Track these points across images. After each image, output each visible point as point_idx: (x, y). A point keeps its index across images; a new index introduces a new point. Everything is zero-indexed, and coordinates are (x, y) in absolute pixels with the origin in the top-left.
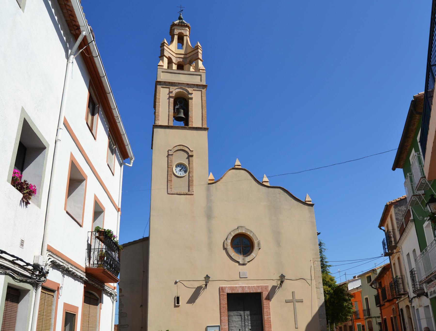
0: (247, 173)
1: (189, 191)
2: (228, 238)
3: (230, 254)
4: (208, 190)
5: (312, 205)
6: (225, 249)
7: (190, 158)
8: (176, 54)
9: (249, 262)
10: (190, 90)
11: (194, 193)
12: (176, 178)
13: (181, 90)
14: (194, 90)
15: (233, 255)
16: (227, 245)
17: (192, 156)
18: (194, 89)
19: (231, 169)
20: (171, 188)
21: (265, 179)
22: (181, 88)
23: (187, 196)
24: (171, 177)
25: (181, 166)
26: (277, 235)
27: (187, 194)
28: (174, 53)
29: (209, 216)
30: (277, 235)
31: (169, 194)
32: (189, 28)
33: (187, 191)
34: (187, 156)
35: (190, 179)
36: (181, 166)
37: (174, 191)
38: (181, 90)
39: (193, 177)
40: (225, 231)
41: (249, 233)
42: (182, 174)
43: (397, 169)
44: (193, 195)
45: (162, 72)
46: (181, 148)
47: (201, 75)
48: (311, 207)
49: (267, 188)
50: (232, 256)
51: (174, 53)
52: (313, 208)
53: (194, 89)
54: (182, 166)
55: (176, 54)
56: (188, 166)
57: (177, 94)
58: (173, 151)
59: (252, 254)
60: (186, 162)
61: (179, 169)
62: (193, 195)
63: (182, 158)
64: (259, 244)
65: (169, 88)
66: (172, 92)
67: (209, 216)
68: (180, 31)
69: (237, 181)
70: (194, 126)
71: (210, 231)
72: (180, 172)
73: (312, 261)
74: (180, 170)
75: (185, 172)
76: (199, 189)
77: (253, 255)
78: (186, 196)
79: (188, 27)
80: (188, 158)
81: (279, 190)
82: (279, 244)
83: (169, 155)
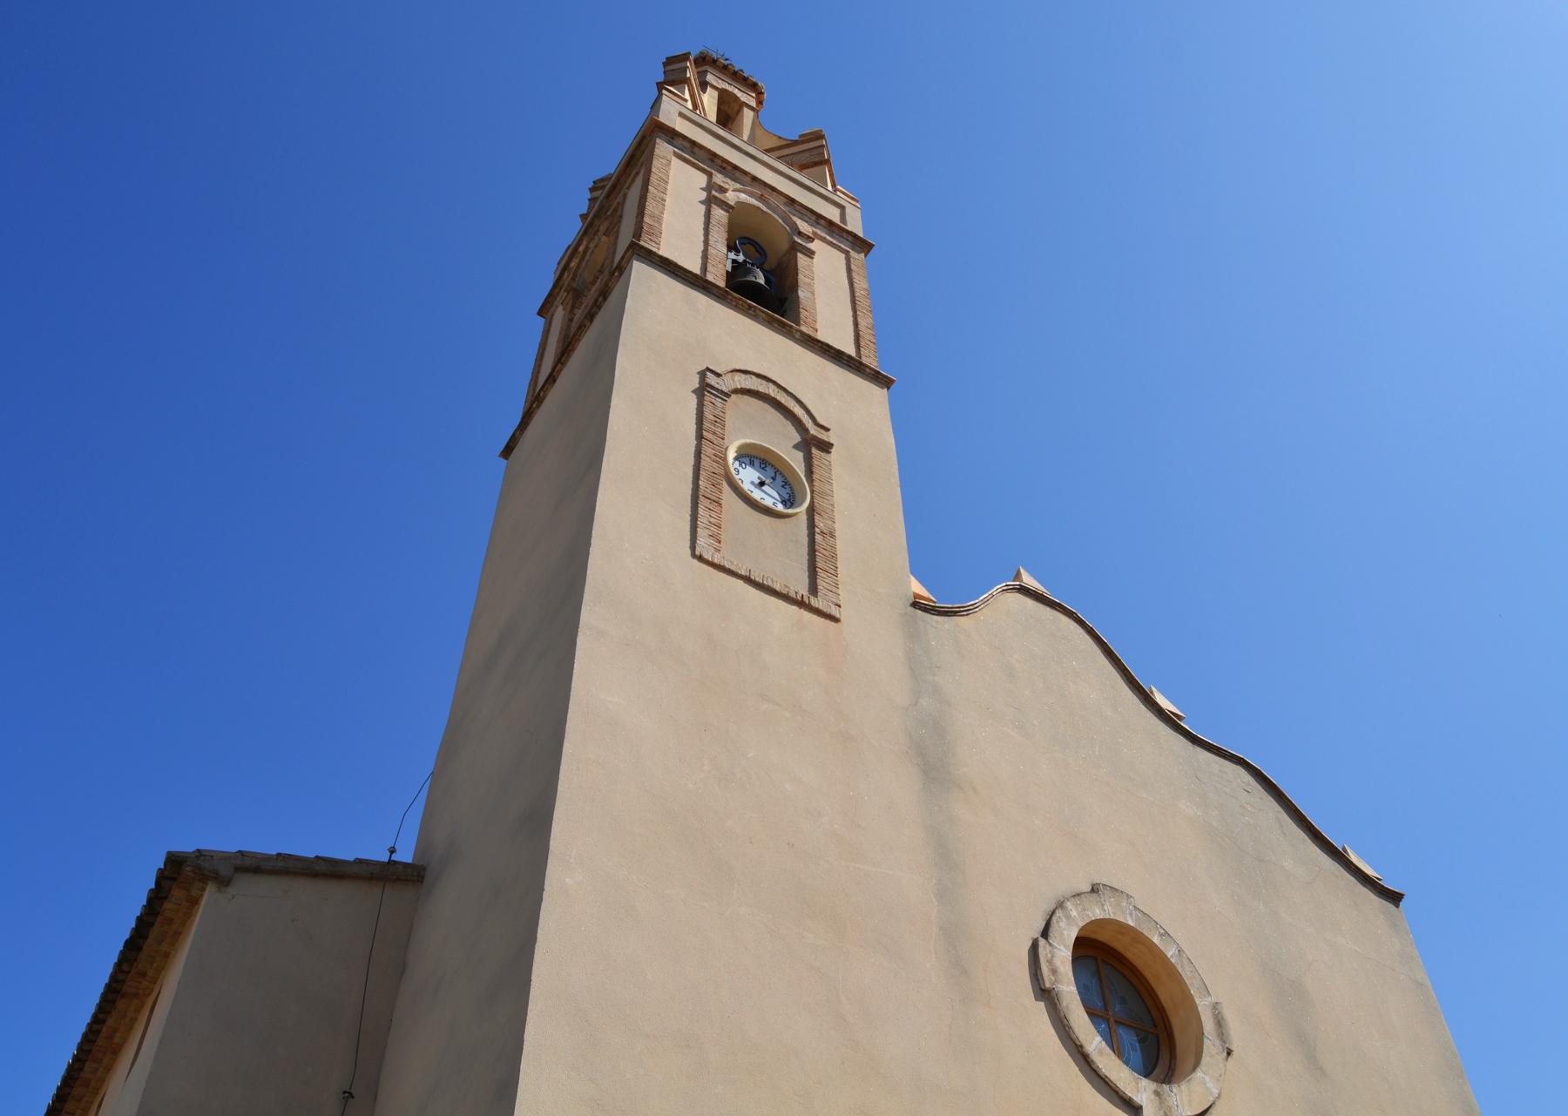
1: (813, 590)
6: (1045, 994)
16: (1054, 971)
22: (761, 198)
34: (797, 438)
41: (1156, 940)
44: (836, 620)
46: (772, 391)
62: (836, 620)
63: (782, 442)
64: (1220, 1023)
71: (945, 856)
74: (762, 484)
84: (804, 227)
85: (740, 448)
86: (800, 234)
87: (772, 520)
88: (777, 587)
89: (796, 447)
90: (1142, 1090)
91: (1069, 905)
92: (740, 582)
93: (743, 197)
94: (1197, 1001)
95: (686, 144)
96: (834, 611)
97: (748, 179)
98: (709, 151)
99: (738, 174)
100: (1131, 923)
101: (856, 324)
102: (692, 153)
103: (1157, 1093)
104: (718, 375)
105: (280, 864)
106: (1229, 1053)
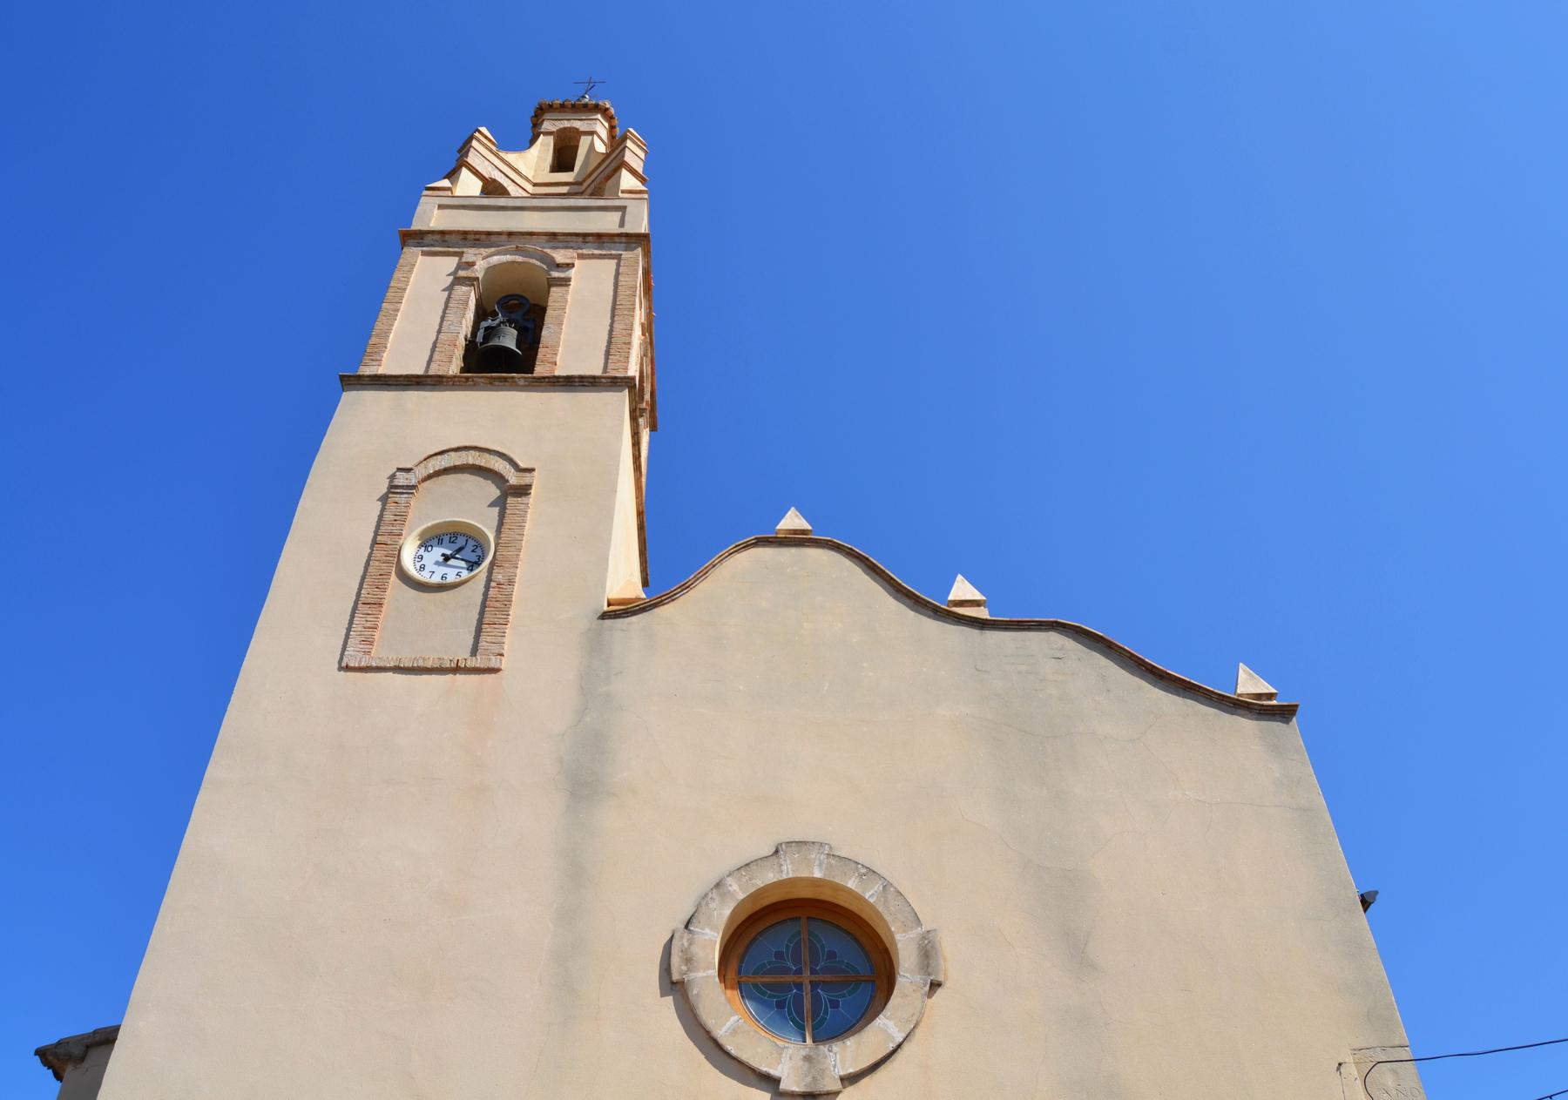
0: (847, 563)
1: (474, 652)
2: (702, 917)
3: (710, 1021)
4: (595, 647)
5: (1285, 713)
6: (674, 987)
7: (510, 500)
8: (535, 185)
9: (851, 1080)
10: (560, 256)
11: (504, 664)
12: (411, 593)
13: (519, 259)
14: (581, 257)
15: (734, 1032)
16: (688, 960)
17: (523, 491)
18: (585, 251)
19: (747, 546)
20: (369, 642)
21: (962, 589)
22: (518, 251)
23: (460, 678)
24: (381, 587)
25: (458, 542)
26: (1064, 908)
27: (457, 670)
28: (527, 179)
29: (584, 781)
30: (1064, 908)
31: (348, 668)
32: (610, 118)
33: (462, 654)
34: (494, 492)
35: (492, 592)
36: (458, 542)
37: (382, 653)
38: (519, 259)
39: (511, 582)
40: (689, 862)
41: (852, 884)
42: (454, 572)
43: (742, 574)
44: (496, 670)
45: (440, 207)
46: (471, 458)
47: (623, 209)
48: (1277, 726)
49: (974, 633)
50: (721, 1033)
51: (527, 179)
52: (1290, 732)
53: (585, 251)
54: (461, 542)
55: (535, 185)
56: (491, 536)
57: (490, 270)
58: (422, 472)
59: (881, 1021)
60: (485, 522)
61: (437, 553)
62: (496, 670)
63: (470, 504)
64: (928, 953)
65: (460, 254)
66: (472, 264)
67: (584, 781)
68: (566, 124)
69: (789, 602)
70: (559, 372)
71: (575, 873)
72: (443, 570)
73: (1351, 1070)
74: (447, 558)
75: (472, 565)
76: (539, 642)
77: (886, 1027)
78: (450, 676)
79: (604, 111)
80: (500, 503)
81: (1054, 637)
82: (1078, 954)
83: (393, 488)
84: (560, 256)
85: (421, 535)
86: (558, 266)
87: (451, 593)
88: (429, 664)
89: (492, 505)
90: (786, 1058)
91: (729, 880)
92: (390, 674)
93: (496, 259)
94: (898, 937)
95: (437, 237)
96: (494, 663)
97: (504, 237)
98: (458, 232)
99: (493, 238)
100: (818, 874)
101: (611, 331)
102: (444, 243)
103: (808, 1059)
104: (409, 470)
105: (97, 1038)
106: (935, 985)
